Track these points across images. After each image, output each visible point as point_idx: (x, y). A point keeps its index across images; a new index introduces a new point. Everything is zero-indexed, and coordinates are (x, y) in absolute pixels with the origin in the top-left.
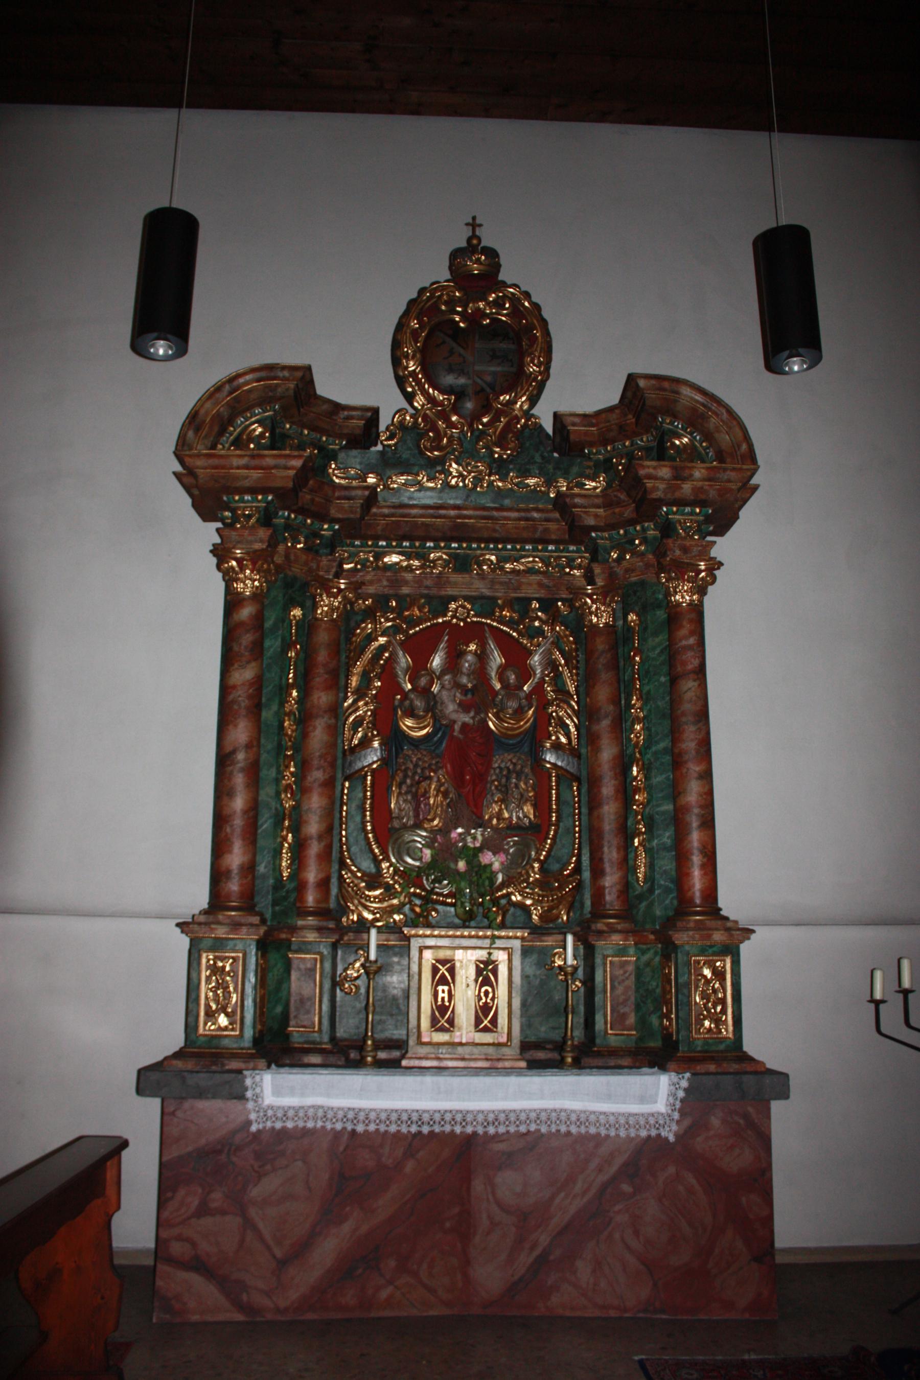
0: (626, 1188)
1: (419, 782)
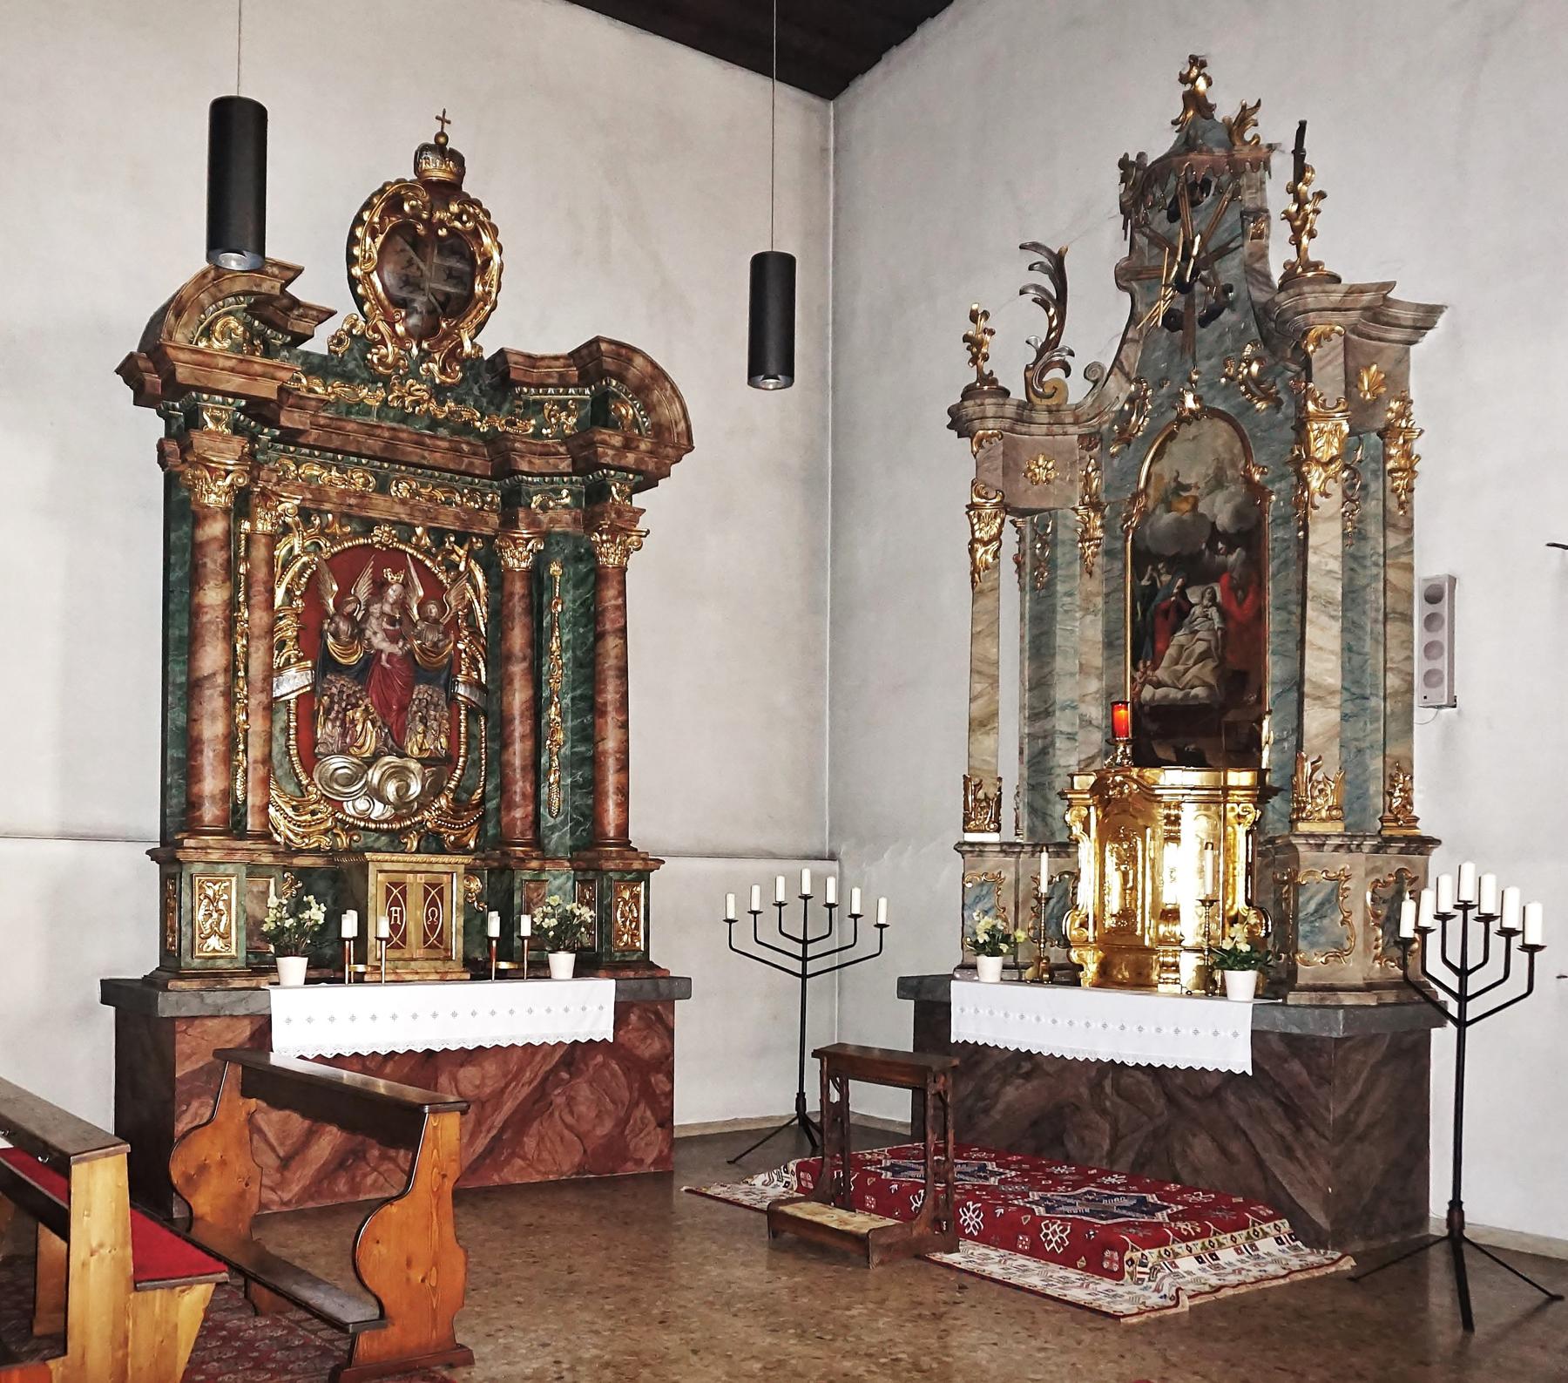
0: (565, 1076)
1: (346, 710)
